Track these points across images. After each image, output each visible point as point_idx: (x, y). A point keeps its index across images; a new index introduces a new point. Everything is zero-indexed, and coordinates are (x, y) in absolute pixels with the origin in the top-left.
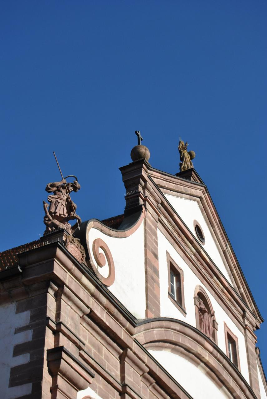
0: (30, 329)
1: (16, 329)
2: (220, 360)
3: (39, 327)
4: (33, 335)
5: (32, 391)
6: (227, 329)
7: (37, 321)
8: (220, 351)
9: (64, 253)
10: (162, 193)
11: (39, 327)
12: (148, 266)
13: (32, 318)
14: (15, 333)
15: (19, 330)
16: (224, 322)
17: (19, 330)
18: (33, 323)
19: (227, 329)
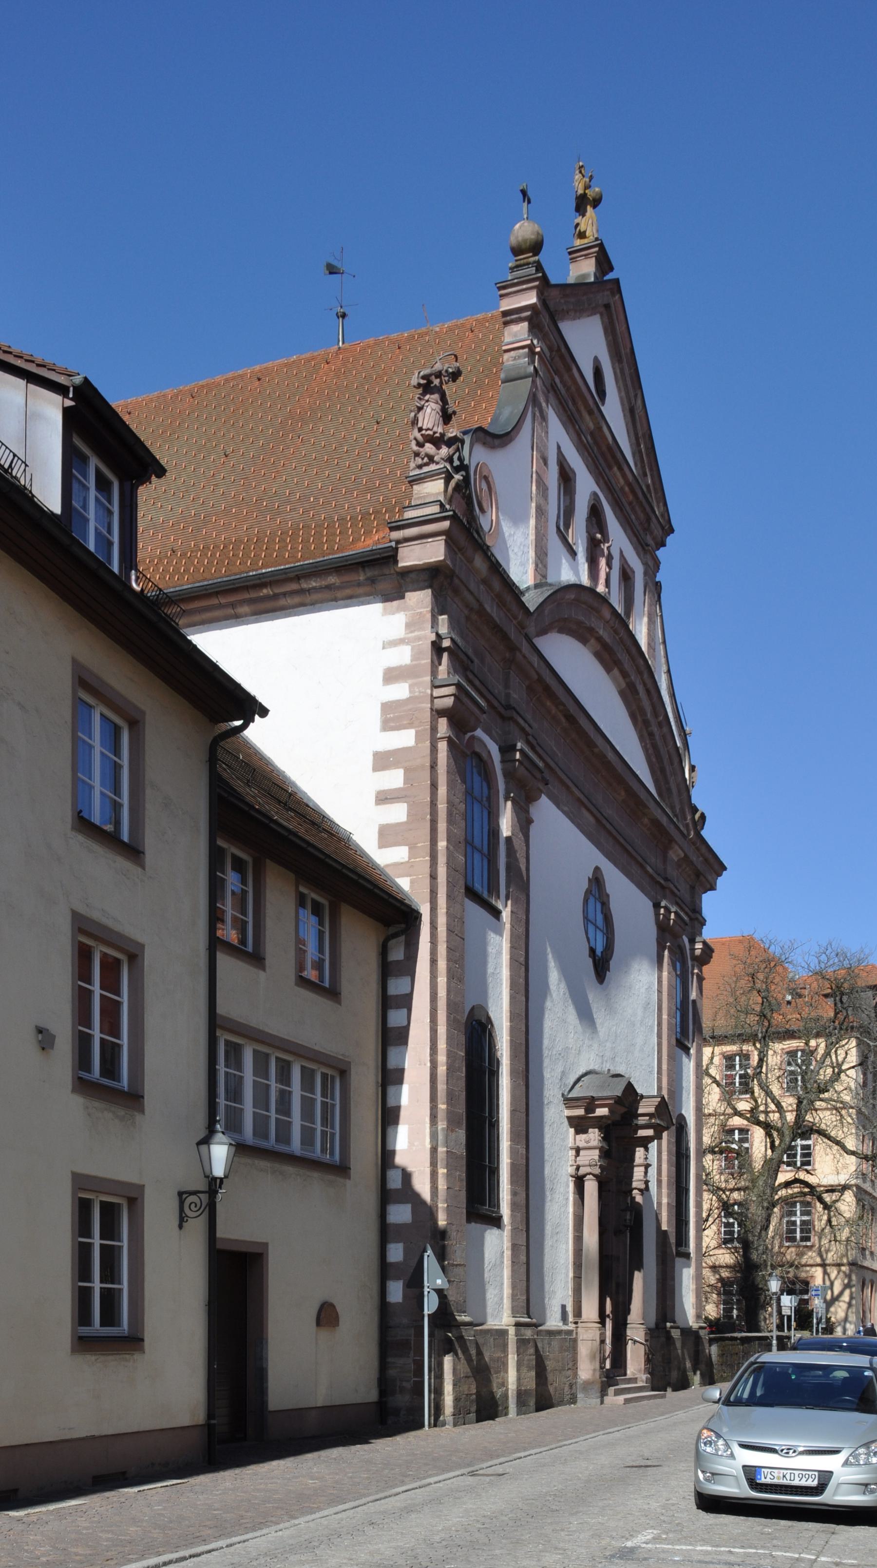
0: (408, 644)
1: (384, 642)
2: (270, 614)
3: (421, 642)
4: (412, 656)
5: (415, 742)
6: (593, 996)
7: (416, 633)
8: (599, 741)
9: (559, 676)
10: (598, 820)
11: (421, 642)
12: (500, 514)
13: (409, 626)
14: (384, 648)
15: (389, 644)
16: (558, 443)
17: (389, 644)
18: (410, 635)
19: (593, 996)
